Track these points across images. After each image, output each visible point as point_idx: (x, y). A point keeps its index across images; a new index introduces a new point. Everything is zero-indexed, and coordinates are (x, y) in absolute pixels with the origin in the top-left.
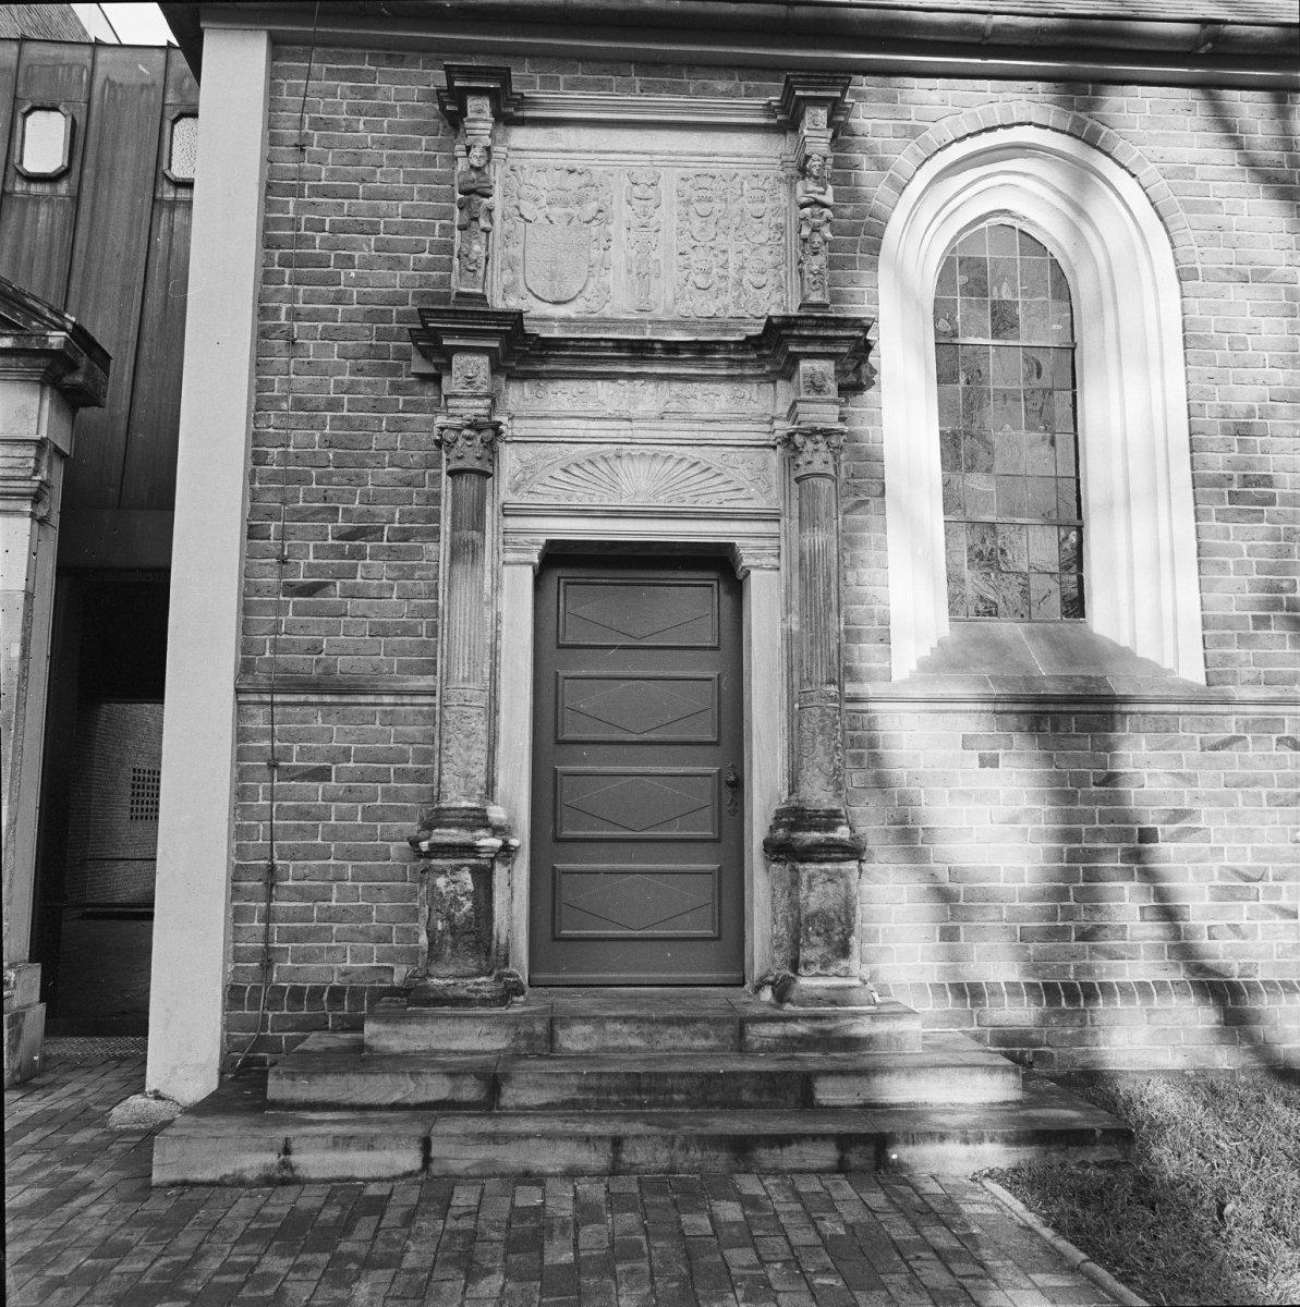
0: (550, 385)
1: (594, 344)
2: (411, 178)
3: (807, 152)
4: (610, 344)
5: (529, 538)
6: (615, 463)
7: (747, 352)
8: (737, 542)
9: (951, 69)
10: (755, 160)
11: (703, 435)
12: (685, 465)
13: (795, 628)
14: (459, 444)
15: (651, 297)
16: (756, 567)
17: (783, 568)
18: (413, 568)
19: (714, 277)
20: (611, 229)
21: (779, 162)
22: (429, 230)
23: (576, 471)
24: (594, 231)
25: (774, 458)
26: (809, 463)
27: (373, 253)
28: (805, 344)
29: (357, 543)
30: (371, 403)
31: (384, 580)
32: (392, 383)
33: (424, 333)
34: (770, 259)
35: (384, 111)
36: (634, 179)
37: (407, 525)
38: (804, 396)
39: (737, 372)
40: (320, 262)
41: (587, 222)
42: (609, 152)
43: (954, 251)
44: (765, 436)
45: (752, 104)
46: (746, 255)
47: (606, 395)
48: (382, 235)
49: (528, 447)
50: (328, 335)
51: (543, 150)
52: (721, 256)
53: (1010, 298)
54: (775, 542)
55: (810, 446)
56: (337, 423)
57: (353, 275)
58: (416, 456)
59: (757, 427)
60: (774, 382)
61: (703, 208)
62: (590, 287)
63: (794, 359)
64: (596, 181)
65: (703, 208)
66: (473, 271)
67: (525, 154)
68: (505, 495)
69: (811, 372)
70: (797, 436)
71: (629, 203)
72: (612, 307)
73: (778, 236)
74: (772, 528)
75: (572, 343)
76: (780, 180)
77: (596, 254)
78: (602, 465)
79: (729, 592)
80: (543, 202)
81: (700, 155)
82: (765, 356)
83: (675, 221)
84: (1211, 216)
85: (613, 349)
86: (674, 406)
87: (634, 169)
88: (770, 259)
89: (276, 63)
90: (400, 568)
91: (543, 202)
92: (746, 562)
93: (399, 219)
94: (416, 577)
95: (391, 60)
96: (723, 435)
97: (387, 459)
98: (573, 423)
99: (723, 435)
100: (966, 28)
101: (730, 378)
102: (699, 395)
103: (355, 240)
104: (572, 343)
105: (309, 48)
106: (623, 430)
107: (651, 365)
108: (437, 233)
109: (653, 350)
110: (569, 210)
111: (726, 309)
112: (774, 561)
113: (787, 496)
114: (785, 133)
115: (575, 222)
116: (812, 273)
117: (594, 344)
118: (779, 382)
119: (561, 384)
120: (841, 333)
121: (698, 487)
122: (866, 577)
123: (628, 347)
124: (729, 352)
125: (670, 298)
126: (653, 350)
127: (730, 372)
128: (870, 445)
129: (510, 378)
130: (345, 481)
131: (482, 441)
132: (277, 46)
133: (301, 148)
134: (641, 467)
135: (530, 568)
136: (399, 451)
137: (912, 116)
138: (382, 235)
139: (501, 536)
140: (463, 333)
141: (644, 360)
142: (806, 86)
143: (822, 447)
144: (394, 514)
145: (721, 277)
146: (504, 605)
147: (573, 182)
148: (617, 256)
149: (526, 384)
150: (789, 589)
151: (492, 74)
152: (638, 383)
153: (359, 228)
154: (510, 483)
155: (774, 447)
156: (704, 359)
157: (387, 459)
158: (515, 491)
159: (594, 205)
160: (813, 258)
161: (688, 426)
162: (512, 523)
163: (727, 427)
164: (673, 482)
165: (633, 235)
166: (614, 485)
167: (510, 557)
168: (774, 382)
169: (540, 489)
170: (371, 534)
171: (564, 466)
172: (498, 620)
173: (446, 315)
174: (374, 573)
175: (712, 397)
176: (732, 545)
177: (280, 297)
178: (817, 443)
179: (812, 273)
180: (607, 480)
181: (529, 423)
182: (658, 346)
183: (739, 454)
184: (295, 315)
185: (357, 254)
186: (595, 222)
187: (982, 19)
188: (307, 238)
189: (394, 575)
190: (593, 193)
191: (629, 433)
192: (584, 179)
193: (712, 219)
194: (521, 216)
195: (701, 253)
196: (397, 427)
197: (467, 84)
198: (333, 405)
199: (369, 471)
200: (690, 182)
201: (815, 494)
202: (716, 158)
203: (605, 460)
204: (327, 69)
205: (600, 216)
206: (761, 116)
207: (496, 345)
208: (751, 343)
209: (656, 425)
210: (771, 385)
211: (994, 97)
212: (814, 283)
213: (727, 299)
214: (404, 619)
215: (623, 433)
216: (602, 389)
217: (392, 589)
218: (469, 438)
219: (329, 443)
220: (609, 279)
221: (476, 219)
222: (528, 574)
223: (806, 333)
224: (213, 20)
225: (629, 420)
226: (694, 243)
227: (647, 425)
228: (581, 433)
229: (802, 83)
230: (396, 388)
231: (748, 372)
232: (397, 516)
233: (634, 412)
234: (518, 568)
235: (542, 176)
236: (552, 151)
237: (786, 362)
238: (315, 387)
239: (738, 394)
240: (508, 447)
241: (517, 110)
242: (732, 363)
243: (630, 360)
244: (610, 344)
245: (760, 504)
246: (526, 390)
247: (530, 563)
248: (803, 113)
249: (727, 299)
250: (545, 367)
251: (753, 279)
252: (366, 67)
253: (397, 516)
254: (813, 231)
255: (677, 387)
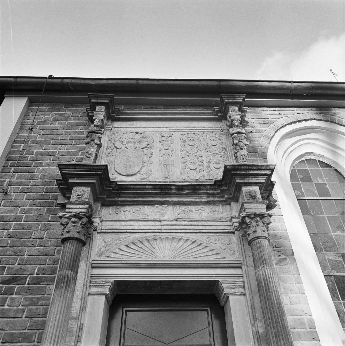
0: (123, 208)
1: (143, 187)
2: (72, 138)
3: (232, 118)
4: (151, 187)
5: (104, 279)
6: (153, 243)
7: (215, 189)
8: (220, 279)
9: (280, 104)
10: (211, 129)
11: (197, 227)
12: (189, 243)
13: (261, 331)
14: (69, 226)
15: (170, 173)
16: (232, 294)
17: (248, 295)
18: (38, 299)
19: (197, 165)
20: (152, 151)
21: (221, 129)
22: (76, 154)
23: (133, 246)
24: (146, 151)
25: (234, 238)
26: (255, 232)
27: (52, 161)
28: (244, 179)
29: (10, 286)
30: (36, 218)
31: (20, 307)
32: (48, 209)
33: (63, 182)
34: (221, 159)
35: (66, 119)
36: (162, 135)
37: (41, 275)
38: (246, 200)
39: (212, 199)
40: (27, 165)
41: (143, 148)
42: (152, 128)
43: (294, 167)
44: (229, 228)
45: (207, 113)
46: (210, 158)
47: (149, 211)
48: (56, 156)
49: (109, 235)
50: (23, 191)
51: (127, 128)
52: (199, 158)
53: (322, 182)
54: (241, 279)
55: (254, 224)
56: (17, 226)
57: (41, 169)
58: (53, 241)
59: (224, 223)
60: (230, 204)
61: (191, 143)
62: (144, 169)
63: (239, 188)
64: (147, 136)
65: (191, 143)
66: (89, 157)
67: (119, 129)
68: (94, 256)
69: (249, 191)
70: (246, 218)
71: (160, 142)
72: (153, 177)
73: (223, 151)
74: (238, 272)
75: (132, 187)
76: (222, 134)
77: (145, 159)
78: (146, 244)
79: (217, 317)
80: (125, 143)
81: (189, 128)
82: (224, 190)
83: (180, 148)
84: (288, 275)
85: (152, 189)
86: (182, 216)
87: (162, 132)
88: (221, 159)
89: (29, 108)
90: (31, 299)
91: (125, 143)
92: (226, 291)
93: (65, 150)
94: (39, 304)
95: (72, 106)
96: (207, 227)
97: (37, 243)
98: (132, 223)
99: (207, 227)
100: (285, 87)
101: (208, 203)
102: (194, 211)
103: (45, 157)
104: (132, 187)
105: (43, 104)
106: (157, 226)
107: (170, 197)
108: (80, 155)
109: (171, 189)
110: (136, 145)
111: (204, 176)
112: (242, 290)
113: (244, 255)
114: (222, 121)
115: (138, 149)
116: (241, 155)
117: (143, 187)
118: (232, 203)
119: (127, 208)
120: (260, 172)
121: (196, 253)
122: (294, 300)
123: (159, 188)
124: (207, 189)
125: (178, 173)
126: (171, 189)
127: (209, 200)
128: (281, 232)
129: (104, 205)
130: (13, 253)
131: (81, 224)
132: (31, 103)
133: (31, 129)
134: (166, 244)
135: (104, 297)
136: (45, 239)
137: (270, 118)
138: (56, 156)
139: (89, 279)
140: (79, 176)
141: (167, 194)
142: (229, 98)
143: (260, 224)
144: (35, 270)
145: (200, 165)
146: (86, 321)
147: (138, 136)
148: (155, 159)
149: (111, 207)
150: (253, 308)
151: (106, 98)
152: (165, 206)
153: (47, 154)
154: (98, 252)
155: (234, 233)
156: (195, 194)
157: (37, 243)
158: (100, 255)
159: (146, 143)
160: (241, 151)
161: (189, 223)
162: (96, 272)
163: (209, 223)
164: (183, 251)
165: (162, 152)
166: (152, 253)
167: (93, 290)
168: (230, 204)
169: (113, 255)
170: (19, 280)
171: (126, 244)
172: (81, 329)
173: (71, 167)
174: (16, 303)
175: (200, 211)
176: (217, 282)
177: (6, 177)
178: (257, 222)
179: (241, 155)
180: (149, 251)
181: (110, 223)
182: (173, 187)
183: (214, 237)
184: (10, 184)
185: (44, 162)
186: (146, 149)
187: (290, 84)
188: (25, 157)
189: (26, 303)
190: (145, 139)
191: (160, 227)
192: (143, 135)
193: (196, 146)
194: (115, 147)
195: (191, 158)
196: (46, 229)
197: (96, 101)
198: (16, 219)
199: (27, 248)
200: (185, 136)
201: (260, 248)
202: (195, 129)
203: (148, 240)
204: (48, 109)
205: (148, 146)
206: (212, 115)
207: (94, 181)
208: (217, 184)
209: (173, 223)
210: (228, 206)
211: (299, 112)
212: (243, 159)
213: (204, 173)
214: (26, 331)
215: (157, 227)
216: (147, 209)
217: (24, 312)
218: (74, 222)
219: (10, 236)
220: (152, 167)
221: (93, 140)
222: (102, 301)
223: (243, 172)
224: (7, 94)
225: (160, 221)
226: (188, 154)
227: (169, 223)
228: (136, 228)
229: (227, 98)
230: (49, 212)
231: (216, 199)
232: (36, 271)
233: (162, 218)
234: (96, 297)
235: (125, 135)
236: (131, 128)
237: (235, 191)
238: (10, 212)
239: (213, 210)
240: (99, 235)
241: (117, 115)
242: (209, 195)
243: (161, 195)
244: (151, 187)
245: (229, 258)
246: (110, 210)
247: (104, 294)
248: (229, 108)
249: (204, 173)
250: (120, 199)
251: (214, 165)
252: (63, 108)
253: (36, 271)
254: (239, 141)
255: (183, 208)
